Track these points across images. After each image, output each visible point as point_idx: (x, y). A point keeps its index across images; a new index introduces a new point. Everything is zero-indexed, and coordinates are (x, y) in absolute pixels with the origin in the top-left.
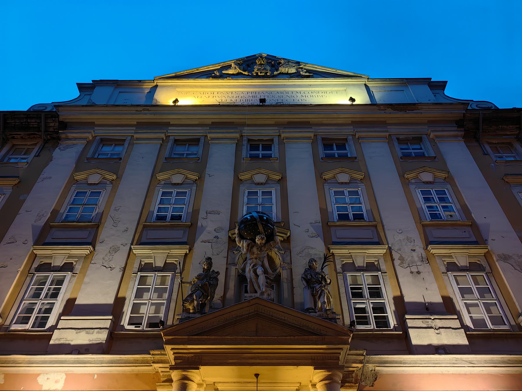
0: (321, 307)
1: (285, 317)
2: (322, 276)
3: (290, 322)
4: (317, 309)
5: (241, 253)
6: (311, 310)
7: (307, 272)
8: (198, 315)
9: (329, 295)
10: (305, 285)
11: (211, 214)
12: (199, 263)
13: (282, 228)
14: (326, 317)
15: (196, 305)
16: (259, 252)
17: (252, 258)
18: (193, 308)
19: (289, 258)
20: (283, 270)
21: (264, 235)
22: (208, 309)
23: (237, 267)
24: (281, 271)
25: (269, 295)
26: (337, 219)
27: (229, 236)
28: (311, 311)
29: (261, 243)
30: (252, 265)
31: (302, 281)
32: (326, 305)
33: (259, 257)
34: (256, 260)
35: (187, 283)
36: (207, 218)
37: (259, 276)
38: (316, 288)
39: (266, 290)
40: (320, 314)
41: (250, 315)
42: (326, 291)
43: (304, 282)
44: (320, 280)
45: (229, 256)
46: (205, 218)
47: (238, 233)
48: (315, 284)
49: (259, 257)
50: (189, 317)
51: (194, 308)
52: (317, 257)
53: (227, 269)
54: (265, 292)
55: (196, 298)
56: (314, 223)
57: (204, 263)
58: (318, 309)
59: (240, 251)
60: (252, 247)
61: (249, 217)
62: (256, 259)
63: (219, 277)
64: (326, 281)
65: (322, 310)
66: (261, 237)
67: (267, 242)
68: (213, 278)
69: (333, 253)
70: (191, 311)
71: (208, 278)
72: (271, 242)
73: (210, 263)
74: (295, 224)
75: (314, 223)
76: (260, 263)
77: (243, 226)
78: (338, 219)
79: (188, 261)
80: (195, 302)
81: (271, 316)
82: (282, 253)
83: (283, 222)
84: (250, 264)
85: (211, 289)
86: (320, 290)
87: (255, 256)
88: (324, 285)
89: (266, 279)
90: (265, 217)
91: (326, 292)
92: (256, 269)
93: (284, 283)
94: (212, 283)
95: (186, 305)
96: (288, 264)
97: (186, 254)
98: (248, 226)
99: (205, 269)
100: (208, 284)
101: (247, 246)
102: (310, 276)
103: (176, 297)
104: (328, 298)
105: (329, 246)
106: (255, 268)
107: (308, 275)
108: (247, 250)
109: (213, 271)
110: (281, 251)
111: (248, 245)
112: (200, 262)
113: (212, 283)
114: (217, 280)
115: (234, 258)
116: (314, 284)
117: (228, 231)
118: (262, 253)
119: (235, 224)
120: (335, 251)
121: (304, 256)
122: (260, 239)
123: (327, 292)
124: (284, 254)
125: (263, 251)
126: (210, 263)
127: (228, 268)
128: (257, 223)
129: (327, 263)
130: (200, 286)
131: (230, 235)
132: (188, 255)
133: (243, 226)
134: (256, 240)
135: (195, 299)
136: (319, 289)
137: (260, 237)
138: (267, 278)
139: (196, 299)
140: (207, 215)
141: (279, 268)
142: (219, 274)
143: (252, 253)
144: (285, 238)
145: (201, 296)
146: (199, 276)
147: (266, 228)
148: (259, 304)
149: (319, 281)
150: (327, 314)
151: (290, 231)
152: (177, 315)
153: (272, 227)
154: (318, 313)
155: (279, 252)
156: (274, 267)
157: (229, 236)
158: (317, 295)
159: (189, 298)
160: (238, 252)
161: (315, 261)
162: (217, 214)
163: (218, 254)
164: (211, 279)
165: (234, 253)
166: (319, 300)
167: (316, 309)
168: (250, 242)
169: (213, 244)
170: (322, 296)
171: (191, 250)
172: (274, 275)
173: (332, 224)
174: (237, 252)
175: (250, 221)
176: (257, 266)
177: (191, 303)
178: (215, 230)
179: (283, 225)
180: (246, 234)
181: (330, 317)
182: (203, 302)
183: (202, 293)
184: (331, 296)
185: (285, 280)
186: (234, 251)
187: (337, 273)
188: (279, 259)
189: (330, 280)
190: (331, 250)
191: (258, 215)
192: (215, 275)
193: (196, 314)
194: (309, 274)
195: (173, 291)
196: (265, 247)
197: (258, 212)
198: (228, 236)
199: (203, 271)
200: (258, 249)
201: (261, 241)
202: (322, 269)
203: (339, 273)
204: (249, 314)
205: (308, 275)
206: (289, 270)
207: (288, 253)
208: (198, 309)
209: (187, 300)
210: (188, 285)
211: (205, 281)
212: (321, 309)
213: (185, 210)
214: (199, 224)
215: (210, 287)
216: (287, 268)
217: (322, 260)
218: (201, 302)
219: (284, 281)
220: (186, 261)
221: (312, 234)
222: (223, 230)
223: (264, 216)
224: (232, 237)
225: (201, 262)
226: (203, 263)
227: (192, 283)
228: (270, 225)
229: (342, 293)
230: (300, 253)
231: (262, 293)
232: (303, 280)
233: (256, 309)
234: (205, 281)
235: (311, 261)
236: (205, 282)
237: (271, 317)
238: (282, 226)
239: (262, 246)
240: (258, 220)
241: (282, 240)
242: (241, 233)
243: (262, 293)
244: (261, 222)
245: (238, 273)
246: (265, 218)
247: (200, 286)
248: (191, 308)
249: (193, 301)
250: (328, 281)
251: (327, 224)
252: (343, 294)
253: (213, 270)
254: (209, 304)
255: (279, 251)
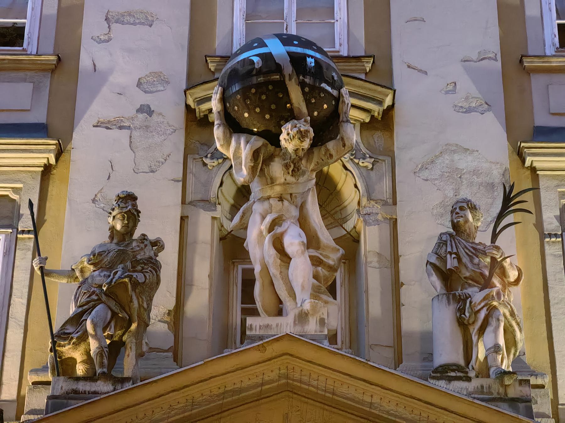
0: (486, 358)
1: (372, 396)
2: (493, 259)
3: (388, 413)
4: (473, 368)
5: (226, 166)
6: (453, 371)
7: (444, 247)
8: (103, 386)
9: (514, 323)
10: (438, 291)
11: (123, 23)
12: (94, 201)
13: (366, 81)
14: (498, 393)
15: (94, 352)
16: (290, 179)
17: (269, 198)
18: (85, 357)
19: (386, 183)
20: (366, 223)
21: (305, 121)
22: (134, 362)
23: (217, 214)
24: (361, 226)
25: (322, 322)
26: (554, 45)
27: (187, 106)
28: (453, 374)
29: (296, 151)
30: (269, 219)
31: (428, 275)
32: (503, 354)
33: (291, 194)
34: (280, 202)
35: (60, 273)
36: (108, 41)
37: (291, 259)
38: (471, 302)
39: (314, 308)
40: (482, 387)
41: (264, 388)
42: (503, 310)
43: (435, 278)
44: (487, 273)
45: (190, 177)
46: (102, 37)
47: (219, 112)
48: (470, 285)
49: (291, 194)
50: (75, 392)
51: (89, 360)
52: (480, 180)
53: (183, 219)
54: (311, 313)
55: (95, 330)
56: (475, 58)
57: (114, 213)
58: (476, 367)
59: (226, 159)
60: (269, 160)
61: (256, 59)
62: (281, 199)
63: (162, 257)
64: (503, 274)
65: (489, 370)
66: (300, 132)
67: (317, 142)
68: (144, 263)
69: (535, 168)
70: (80, 370)
71: (129, 264)
72: (331, 145)
73: (133, 214)
74: (413, 64)
75: (475, 58)
76: (295, 212)
77: (236, 88)
78: (558, 45)
79: (53, 190)
80: (93, 344)
81: (330, 393)
82: (366, 167)
83: (370, 57)
84: (261, 214)
85: (138, 299)
86: (485, 309)
87: (278, 189)
88: (498, 294)
89: (313, 265)
90: (312, 57)
91: (505, 315)
92: (282, 234)
93: (369, 269)
94: (140, 278)
95: (64, 349)
96: (385, 203)
97: (47, 169)
98: (253, 91)
99: (116, 230)
100: (129, 286)
101: (250, 157)
102: (456, 260)
103: (25, 310)
104: (509, 333)
105: (523, 144)
106: (279, 230)
107: (448, 256)
108: (253, 170)
109: (144, 237)
110: (361, 161)
111: (256, 154)
112: (96, 195)
113: (143, 280)
114: (156, 267)
115: (207, 185)
116: (467, 286)
117: (185, 92)
118: (302, 179)
119: (206, 61)
120: (539, 162)
121: (436, 179)
122: (294, 137)
123: (508, 314)
124: (372, 169)
125: (304, 173)
126: (134, 211)
127: (187, 217)
128: (284, 81)
129: (512, 215)
130: (105, 289)
131: (191, 102)
132: (55, 171)
133: (236, 88)
134: (282, 138)
135: (91, 335)
136: (483, 304)
137: (295, 130)
138: (316, 262)
139: (93, 333)
140: (109, 27)
141: (355, 216)
142: (162, 248)
143: (269, 180)
144: (376, 114)
145: (110, 323)
146: (100, 254)
147: (315, 98)
148: (291, 355)
149: (482, 274)
150: (502, 384)
151: (395, 91)
152: (31, 371)
153: (335, 93)
154: (475, 383)
155: (354, 162)
156: (338, 209)
157: (187, 106)
158: (473, 323)
159: (70, 329)
160: (220, 161)
161: (473, 208)
162: (141, 23)
163: (154, 167)
164: (139, 268)
165: (205, 165)
166: (481, 339)
167: (470, 367)
168: (258, 142)
169: (136, 134)
170: (489, 329)
171: (62, 152)
172: (339, 250)
173: (537, 63)
174: (215, 161)
175: (260, 72)
176: (285, 225)
177: (80, 343)
178: (139, 84)
179: (368, 67)
180: (246, 115)
181: (513, 392)
182: (116, 339)
183: (112, 310)
184: (518, 324)
185: (373, 260)
186: (206, 157)
187: (543, 236)
188: (356, 186)
189: (519, 270)
190: (528, 161)
191: (289, 53)
192: (149, 252)
193: (96, 380)
194: (451, 254)
195: (14, 291)
196: (309, 160)
197: (287, 40)
198: (184, 105)
199: (112, 237)
200: (287, 166)
201: (296, 142)
202: (495, 236)
203: (550, 236)
204: (262, 384)
205: (448, 256)
206: (386, 228)
207: (384, 167)
208: (102, 365)
209: (65, 334)
210: (64, 281)
211: (119, 273)
212: (484, 372)
213: (33, 9)
214: (85, 61)
215: (137, 291)
216: (380, 217)
217: (496, 193)
218: (108, 342)
219: (369, 260)
220: (50, 189)
221: (467, 98)
222: (168, 83)
223: (309, 56)
224: (197, 110)
225: (99, 196)
226: (110, 213)
227: (78, 273)
228: (329, 89)
229: (556, 301)
230: (424, 168)
231: (302, 317)
232: (434, 273)
233: (282, 371)
234: (119, 273)
235: (462, 208)
236: (120, 278)
237: (331, 396)
238: (368, 70)
239: (301, 159)
240: (288, 69)
241: (367, 120)
242: (230, 111)
243: (302, 317)
244: (299, 78)
245: (221, 230)
246: (310, 62)
247: (105, 289)
248: (78, 355)
249: (84, 337)
250: (513, 275)
251: (521, 61)
252: (557, 303)
253: (144, 235)
254: (134, 348)
255: (356, 161)
